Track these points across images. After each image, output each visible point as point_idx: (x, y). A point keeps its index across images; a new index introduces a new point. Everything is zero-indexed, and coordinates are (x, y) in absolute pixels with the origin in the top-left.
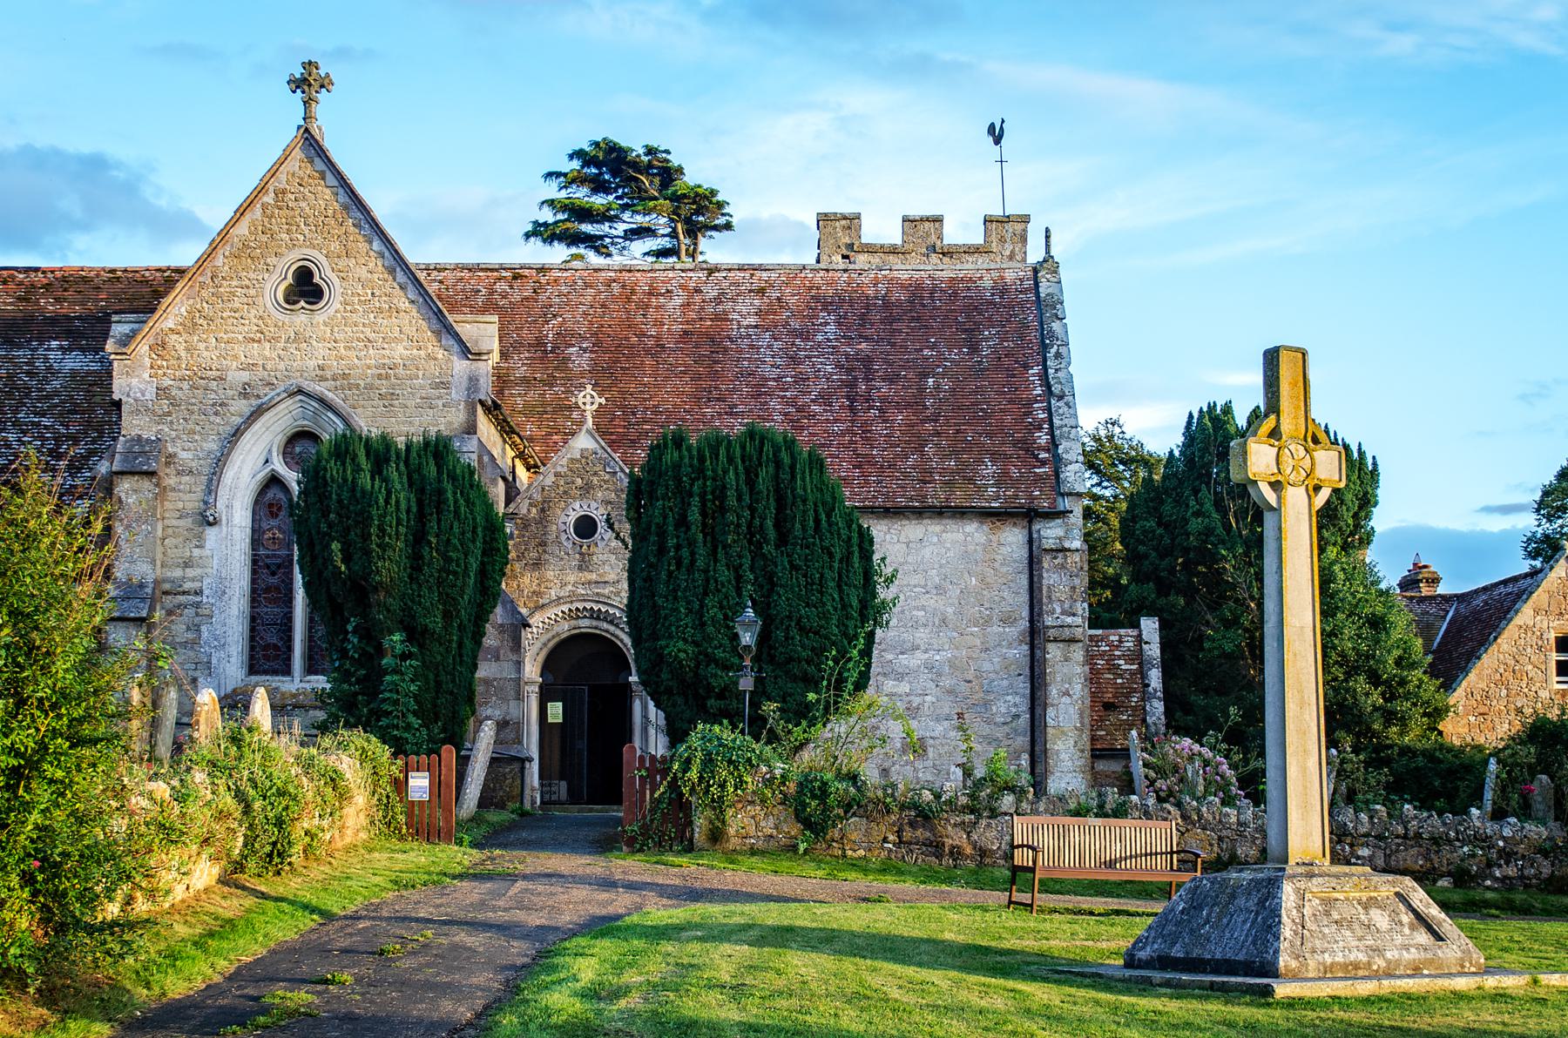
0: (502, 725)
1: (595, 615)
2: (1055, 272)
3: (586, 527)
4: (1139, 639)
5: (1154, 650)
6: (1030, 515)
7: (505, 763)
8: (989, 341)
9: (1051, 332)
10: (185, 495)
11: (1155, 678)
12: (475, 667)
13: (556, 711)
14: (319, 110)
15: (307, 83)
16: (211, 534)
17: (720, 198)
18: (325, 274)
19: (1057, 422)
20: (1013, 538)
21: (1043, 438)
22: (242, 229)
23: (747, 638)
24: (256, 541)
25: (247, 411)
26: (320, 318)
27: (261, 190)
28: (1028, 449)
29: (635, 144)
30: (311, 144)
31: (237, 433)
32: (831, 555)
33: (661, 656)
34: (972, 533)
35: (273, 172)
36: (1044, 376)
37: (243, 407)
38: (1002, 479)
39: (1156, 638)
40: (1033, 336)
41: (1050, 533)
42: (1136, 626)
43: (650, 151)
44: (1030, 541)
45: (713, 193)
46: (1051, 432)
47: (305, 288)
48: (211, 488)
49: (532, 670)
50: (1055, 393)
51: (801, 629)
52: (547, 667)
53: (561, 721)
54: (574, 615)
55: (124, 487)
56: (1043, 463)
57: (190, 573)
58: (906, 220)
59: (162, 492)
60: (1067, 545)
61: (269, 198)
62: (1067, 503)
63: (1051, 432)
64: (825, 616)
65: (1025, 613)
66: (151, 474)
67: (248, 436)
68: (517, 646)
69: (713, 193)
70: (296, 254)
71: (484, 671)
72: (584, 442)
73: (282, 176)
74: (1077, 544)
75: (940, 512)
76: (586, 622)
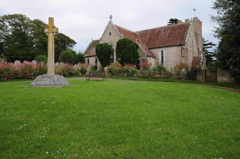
6: (181, 45)
15: (111, 17)
18: (111, 33)
20: (180, 48)
22: (106, 30)
28: (183, 39)
29: (174, 18)
34: (176, 48)
43: (175, 19)
47: (110, 34)
75: (173, 46)
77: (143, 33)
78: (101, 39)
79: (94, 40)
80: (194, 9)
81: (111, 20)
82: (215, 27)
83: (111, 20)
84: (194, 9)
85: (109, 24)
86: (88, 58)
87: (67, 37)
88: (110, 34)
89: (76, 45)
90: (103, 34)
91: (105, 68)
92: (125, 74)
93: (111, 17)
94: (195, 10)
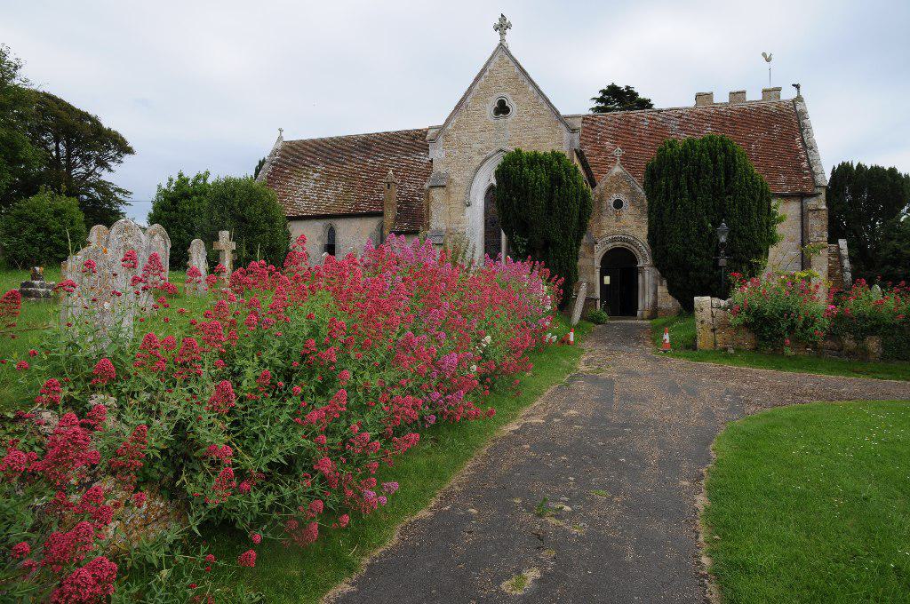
0: (588, 284)
1: (622, 240)
2: (802, 101)
3: (618, 204)
4: (839, 249)
5: (845, 252)
7: (589, 301)
8: (777, 129)
9: (803, 123)
10: (458, 195)
11: (846, 263)
12: (577, 259)
13: (607, 280)
14: (506, 37)
15: (503, 26)
16: (468, 209)
17: (651, 102)
18: (510, 103)
19: (810, 158)
21: (805, 165)
22: (477, 87)
23: (723, 239)
24: (486, 213)
25: (481, 160)
26: (509, 120)
27: (483, 70)
28: (799, 170)
29: (622, 85)
30: (502, 47)
31: (478, 169)
32: (754, 199)
33: (666, 252)
35: (488, 63)
36: (802, 141)
37: (479, 159)
38: (788, 182)
39: (846, 247)
40: (796, 126)
41: (811, 203)
42: (837, 243)
43: (628, 88)
44: (802, 207)
45: (650, 100)
46: (808, 162)
47: (502, 109)
48: (470, 187)
49: (597, 264)
50: (808, 147)
51: (740, 237)
52: (603, 262)
53: (696, 298)
54: (613, 240)
55: (434, 192)
56: (806, 175)
57: (460, 225)
58: (731, 93)
59: (449, 194)
60: (819, 207)
61: (487, 74)
62: (819, 190)
63: (808, 162)
64: (752, 230)
65: (799, 237)
66: (443, 186)
67: (481, 170)
68: (592, 252)
69: (650, 100)
70: (496, 95)
71: (581, 262)
72: (617, 169)
73: (492, 64)
74: (824, 207)
76: (619, 243)
77: (613, 135)
78: (441, 129)
79: (293, 135)
80: (764, 55)
81: (503, 40)
82: (110, 170)
83: (503, 40)
84: (764, 55)
85: (496, 59)
86: (327, 222)
87: (85, 116)
88: (502, 109)
89: (127, 158)
90: (458, 107)
91: (703, 302)
92: (873, 344)
93: (503, 26)
94: (768, 60)
